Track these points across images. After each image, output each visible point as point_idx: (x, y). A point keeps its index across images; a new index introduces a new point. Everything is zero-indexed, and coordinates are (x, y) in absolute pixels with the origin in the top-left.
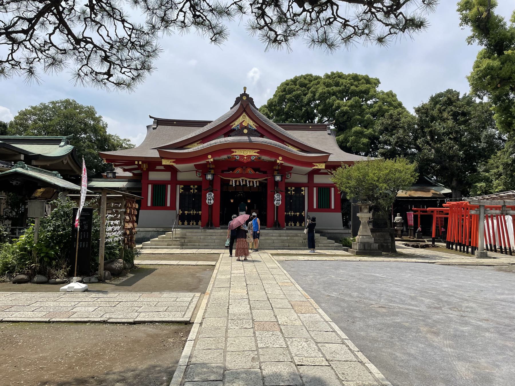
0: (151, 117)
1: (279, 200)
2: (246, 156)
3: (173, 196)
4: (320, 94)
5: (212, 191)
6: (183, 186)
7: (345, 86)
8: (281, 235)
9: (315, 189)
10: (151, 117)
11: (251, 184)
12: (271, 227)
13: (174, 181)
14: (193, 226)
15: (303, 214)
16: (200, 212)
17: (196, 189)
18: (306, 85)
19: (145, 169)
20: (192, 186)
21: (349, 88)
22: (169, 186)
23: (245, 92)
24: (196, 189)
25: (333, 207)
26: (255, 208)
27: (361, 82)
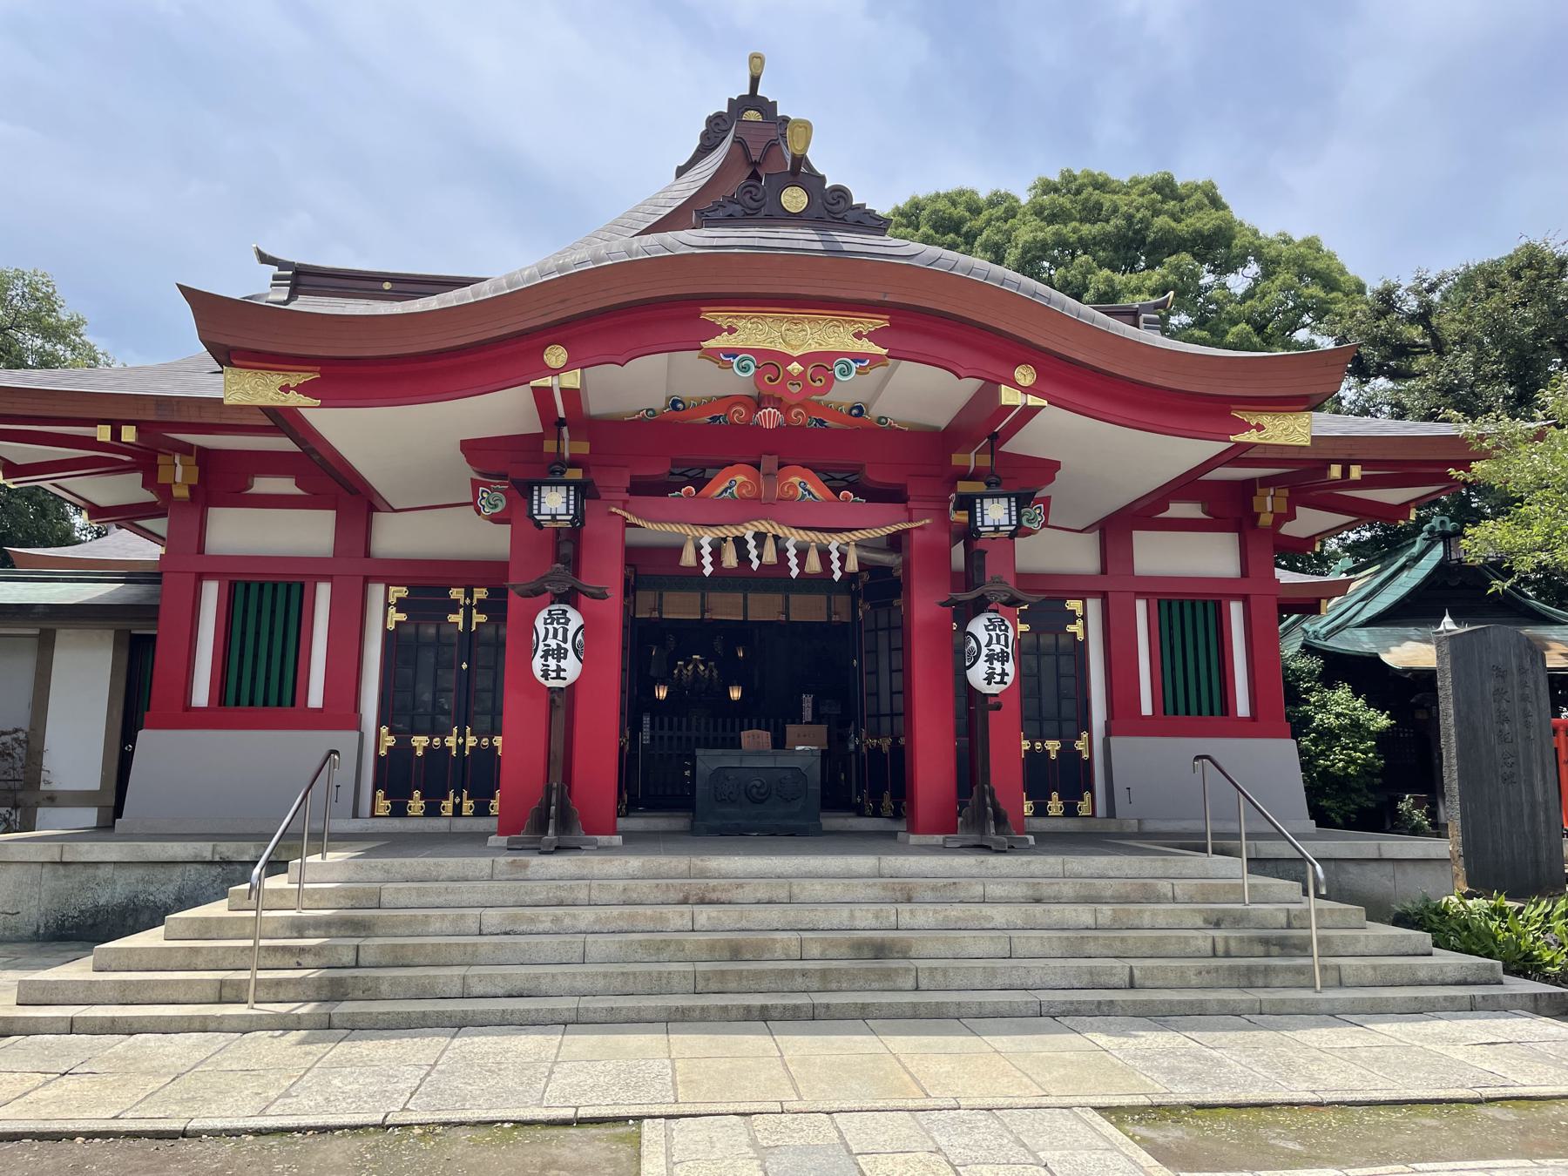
0: (264, 259)
2: (802, 360)
3: (349, 648)
4: (1025, 251)
5: (570, 598)
6: (402, 592)
7: (1129, 218)
8: (1047, 891)
10: (264, 259)
12: (946, 826)
13: (355, 566)
14: (460, 824)
15: (1080, 745)
16: (498, 741)
17: (482, 607)
18: (962, 221)
19: (181, 492)
20: (456, 594)
21: (1146, 223)
22: (324, 591)
23: (755, 81)
24: (482, 607)
25: (1243, 708)
26: (808, 714)
27: (1190, 203)
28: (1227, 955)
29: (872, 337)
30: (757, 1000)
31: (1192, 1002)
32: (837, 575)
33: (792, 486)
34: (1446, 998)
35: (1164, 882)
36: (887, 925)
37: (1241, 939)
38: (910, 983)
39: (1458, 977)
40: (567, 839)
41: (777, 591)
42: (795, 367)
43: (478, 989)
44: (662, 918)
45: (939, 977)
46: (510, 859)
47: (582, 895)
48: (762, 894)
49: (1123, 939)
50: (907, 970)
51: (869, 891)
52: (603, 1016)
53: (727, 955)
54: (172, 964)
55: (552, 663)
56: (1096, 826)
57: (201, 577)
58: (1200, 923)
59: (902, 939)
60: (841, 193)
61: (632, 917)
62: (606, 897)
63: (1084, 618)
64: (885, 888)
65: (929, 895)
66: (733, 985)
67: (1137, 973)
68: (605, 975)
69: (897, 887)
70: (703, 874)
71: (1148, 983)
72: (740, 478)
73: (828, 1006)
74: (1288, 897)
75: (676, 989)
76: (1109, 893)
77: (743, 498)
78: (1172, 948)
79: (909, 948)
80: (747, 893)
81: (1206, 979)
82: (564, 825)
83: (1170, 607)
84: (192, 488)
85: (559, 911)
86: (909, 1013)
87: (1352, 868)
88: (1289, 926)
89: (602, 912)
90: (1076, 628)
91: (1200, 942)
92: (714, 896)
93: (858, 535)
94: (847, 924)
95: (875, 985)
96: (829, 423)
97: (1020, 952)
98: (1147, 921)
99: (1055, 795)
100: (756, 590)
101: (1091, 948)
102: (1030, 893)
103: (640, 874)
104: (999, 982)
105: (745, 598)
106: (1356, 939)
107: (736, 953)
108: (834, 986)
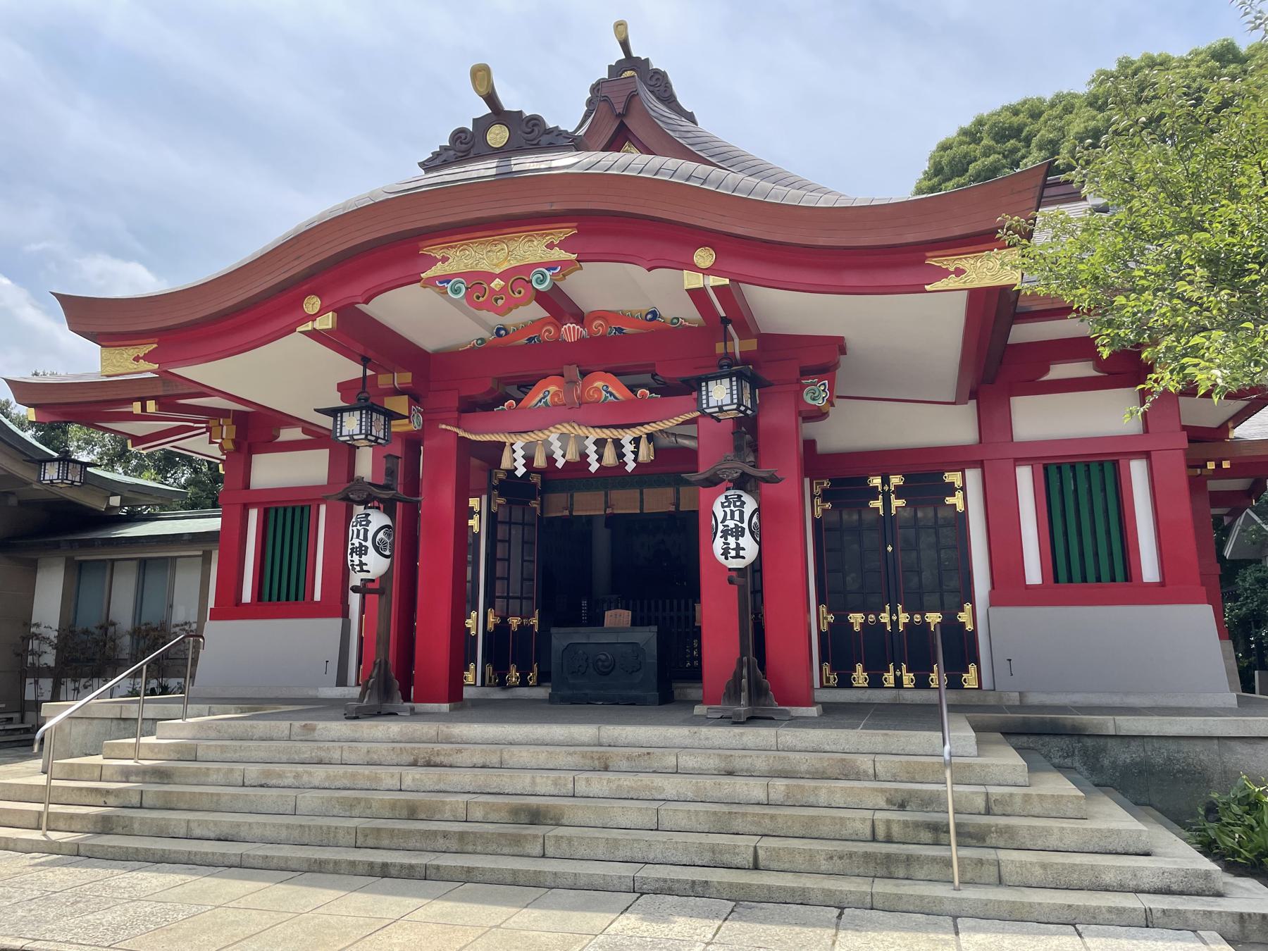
1: (738, 533)
2: (501, 276)
8: (739, 763)
9: (1024, 475)
11: (610, 458)
15: (964, 617)
18: (1019, 130)
23: (625, 45)
25: (1150, 571)
28: (889, 840)
29: (562, 245)
30: (379, 857)
31: (793, 890)
32: (631, 466)
33: (597, 390)
34: (1110, 910)
35: (860, 758)
36: (564, 791)
37: (906, 824)
38: (537, 850)
39: (1158, 883)
40: (388, 707)
41: (669, 485)
42: (497, 284)
43: (197, 832)
44: (376, 778)
45: (564, 845)
46: (303, 723)
47: (336, 756)
48: (478, 759)
49: (772, 817)
50: (535, 837)
51: (569, 758)
52: (259, 863)
53: (405, 813)
54: (33, 798)
55: (731, 540)
56: (975, 698)
57: (246, 508)
58: (883, 804)
59: (555, 807)
60: (536, 121)
61: (353, 775)
62: (354, 758)
63: (963, 489)
64: (584, 756)
65: (624, 765)
66: (386, 843)
67: (761, 852)
68: (288, 827)
69: (596, 756)
70: (448, 740)
71: (774, 865)
72: (553, 389)
73: (438, 868)
74: (1010, 778)
75: (341, 843)
76: (804, 768)
77: (555, 405)
78: (825, 830)
79: (562, 815)
80: (464, 758)
81: (838, 865)
82: (757, 693)
83: (1102, 470)
84: (234, 442)
85: (300, 768)
86: (509, 880)
87: (1238, 747)
88: (988, 812)
89: (332, 770)
90: (956, 500)
91: (858, 825)
92: (438, 760)
93: (649, 429)
94: (529, 790)
95: (506, 850)
96: (627, 330)
97: (666, 824)
98: (823, 798)
99: (859, 667)
100: (650, 486)
101: (738, 824)
102: (723, 765)
103: (398, 738)
104: (621, 854)
105: (642, 493)
106: (1048, 831)
107: (412, 813)
108: (470, 848)
